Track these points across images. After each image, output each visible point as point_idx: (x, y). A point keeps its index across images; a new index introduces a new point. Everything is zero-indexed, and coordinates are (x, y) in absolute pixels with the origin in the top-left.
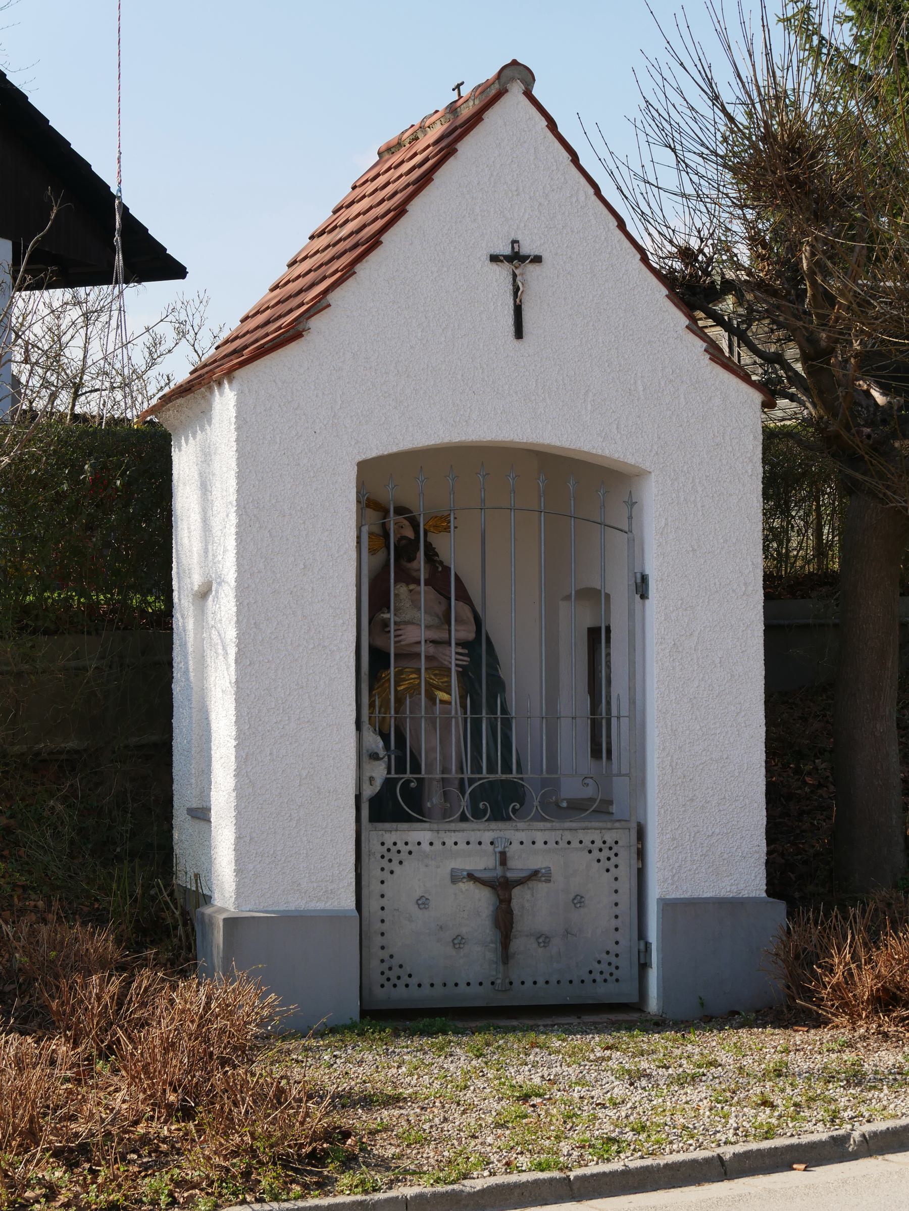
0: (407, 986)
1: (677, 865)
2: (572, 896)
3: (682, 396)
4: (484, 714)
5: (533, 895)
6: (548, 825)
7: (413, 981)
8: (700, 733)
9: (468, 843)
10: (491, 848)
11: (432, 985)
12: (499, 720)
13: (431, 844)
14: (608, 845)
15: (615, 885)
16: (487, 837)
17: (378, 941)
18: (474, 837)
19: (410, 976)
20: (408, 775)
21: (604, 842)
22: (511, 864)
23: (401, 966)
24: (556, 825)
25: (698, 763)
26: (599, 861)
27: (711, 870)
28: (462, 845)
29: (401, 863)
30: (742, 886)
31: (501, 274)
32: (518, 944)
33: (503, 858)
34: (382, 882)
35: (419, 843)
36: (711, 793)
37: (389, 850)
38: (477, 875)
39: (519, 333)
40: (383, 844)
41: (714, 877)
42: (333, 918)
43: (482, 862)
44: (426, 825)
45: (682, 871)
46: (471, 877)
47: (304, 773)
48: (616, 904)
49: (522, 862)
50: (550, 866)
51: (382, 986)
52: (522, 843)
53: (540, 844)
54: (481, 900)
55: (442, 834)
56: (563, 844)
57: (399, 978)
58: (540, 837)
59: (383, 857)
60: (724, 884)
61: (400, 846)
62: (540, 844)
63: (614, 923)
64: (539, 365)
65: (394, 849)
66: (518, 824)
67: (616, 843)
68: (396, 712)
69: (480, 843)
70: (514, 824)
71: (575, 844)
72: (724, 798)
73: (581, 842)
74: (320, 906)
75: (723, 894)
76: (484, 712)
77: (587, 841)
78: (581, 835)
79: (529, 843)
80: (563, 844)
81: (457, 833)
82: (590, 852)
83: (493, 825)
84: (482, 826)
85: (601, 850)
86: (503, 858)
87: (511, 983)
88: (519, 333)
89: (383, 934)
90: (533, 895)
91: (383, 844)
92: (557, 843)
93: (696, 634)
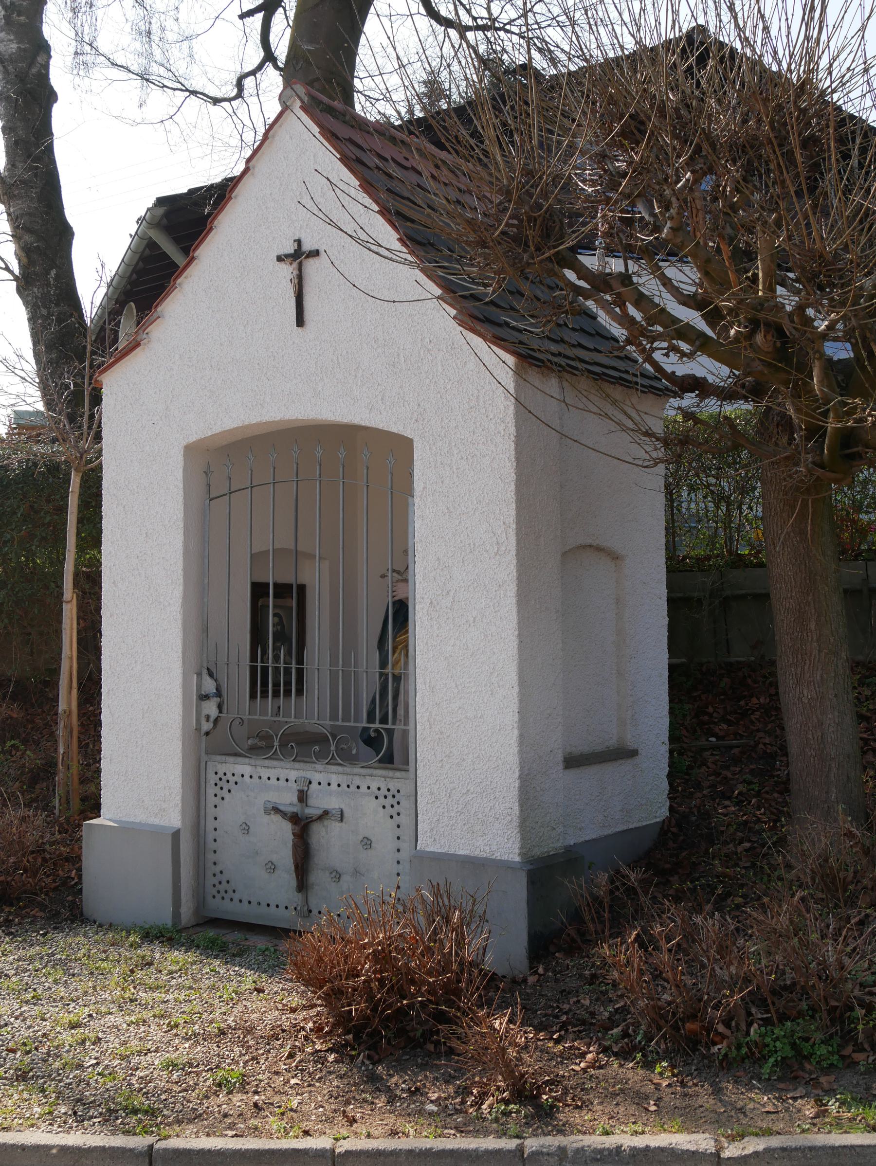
0: (232, 900)
1: (435, 819)
2: (361, 838)
3: (439, 364)
4: (340, 667)
5: (327, 832)
6: (340, 769)
7: (236, 897)
8: (456, 691)
9: (278, 779)
10: (295, 785)
11: (250, 902)
12: (270, 669)
13: (251, 777)
14: (391, 793)
15: (398, 832)
16: (293, 775)
17: (211, 857)
18: (283, 774)
19: (234, 891)
20: (377, 725)
21: (389, 790)
22: (312, 801)
23: (228, 882)
24: (348, 769)
25: (454, 720)
26: (384, 807)
27: (466, 827)
28: (273, 781)
29: (229, 791)
30: (494, 847)
31: (287, 271)
32: (318, 877)
33: (303, 797)
34: (216, 806)
35: (243, 776)
36: (466, 752)
37: (220, 779)
38: (282, 808)
39: (300, 321)
40: (216, 773)
41: (469, 835)
42: (155, 832)
43: (288, 799)
44: (247, 760)
45: (440, 825)
46: (276, 810)
47: (146, 707)
48: (398, 850)
49: (320, 801)
50: (343, 807)
51: (214, 897)
52: (320, 784)
53: (334, 786)
54: (286, 830)
55: (259, 769)
56: (353, 788)
57: (226, 892)
58: (335, 779)
59: (216, 785)
60: (479, 843)
61: (229, 775)
62: (334, 786)
63: (396, 868)
64: (319, 348)
65: (224, 778)
66: (317, 766)
67: (398, 791)
68: (262, 662)
69: (287, 780)
70: (313, 765)
71: (364, 789)
72: (478, 757)
73: (369, 788)
74: (156, 821)
75: (476, 853)
76: (294, 662)
77: (374, 787)
78: (368, 781)
79: (329, 785)
80: (353, 788)
81: (270, 770)
82: (377, 798)
83: (297, 765)
84: (289, 765)
85: (386, 797)
86: (303, 797)
87: (310, 911)
88: (300, 321)
89: (215, 852)
90: (327, 832)
91: (216, 773)
92: (348, 786)
93: (451, 594)
